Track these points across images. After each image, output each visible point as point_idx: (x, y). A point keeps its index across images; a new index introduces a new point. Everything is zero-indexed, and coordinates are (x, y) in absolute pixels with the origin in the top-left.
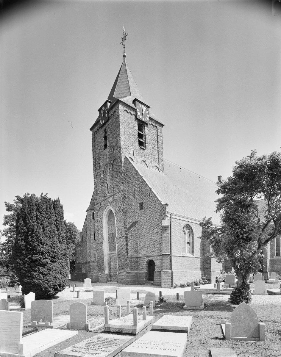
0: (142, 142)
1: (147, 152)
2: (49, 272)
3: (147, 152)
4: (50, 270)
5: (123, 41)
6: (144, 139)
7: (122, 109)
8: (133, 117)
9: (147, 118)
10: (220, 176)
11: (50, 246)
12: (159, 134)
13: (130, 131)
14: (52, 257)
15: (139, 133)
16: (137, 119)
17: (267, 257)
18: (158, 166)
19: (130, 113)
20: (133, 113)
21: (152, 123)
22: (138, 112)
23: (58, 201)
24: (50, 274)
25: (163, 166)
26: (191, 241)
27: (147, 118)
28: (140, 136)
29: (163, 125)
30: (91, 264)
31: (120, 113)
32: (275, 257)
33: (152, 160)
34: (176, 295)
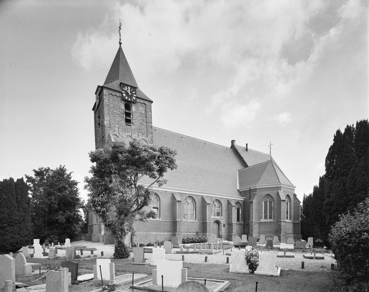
0: (129, 119)
1: (134, 127)
2: (7, 233)
3: (134, 127)
4: (7, 231)
5: (120, 30)
6: (131, 116)
7: (106, 93)
8: (119, 99)
9: (134, 98)
10: (233, 140)
11: (8, 214)
12: (147, 110)
13: (115, 111)
14: (10, 222)
15: (126, 113)
16: (123, 99)
17: (253, 220)
18: (146, 139)
19: (116, 95)
20: (118, 94)
21: (140, 101)
22: (124, 93)
23: (61, 172)
24: (7, 235)
25: (152, 139)
26: (159, 207)
27: (134, 98)
28: (128, 114)
29: (152, 102)
30: (94, 226)
31: (104, 97)
32: (263, 220)
33: (140, 134)
34: (301, 263)
